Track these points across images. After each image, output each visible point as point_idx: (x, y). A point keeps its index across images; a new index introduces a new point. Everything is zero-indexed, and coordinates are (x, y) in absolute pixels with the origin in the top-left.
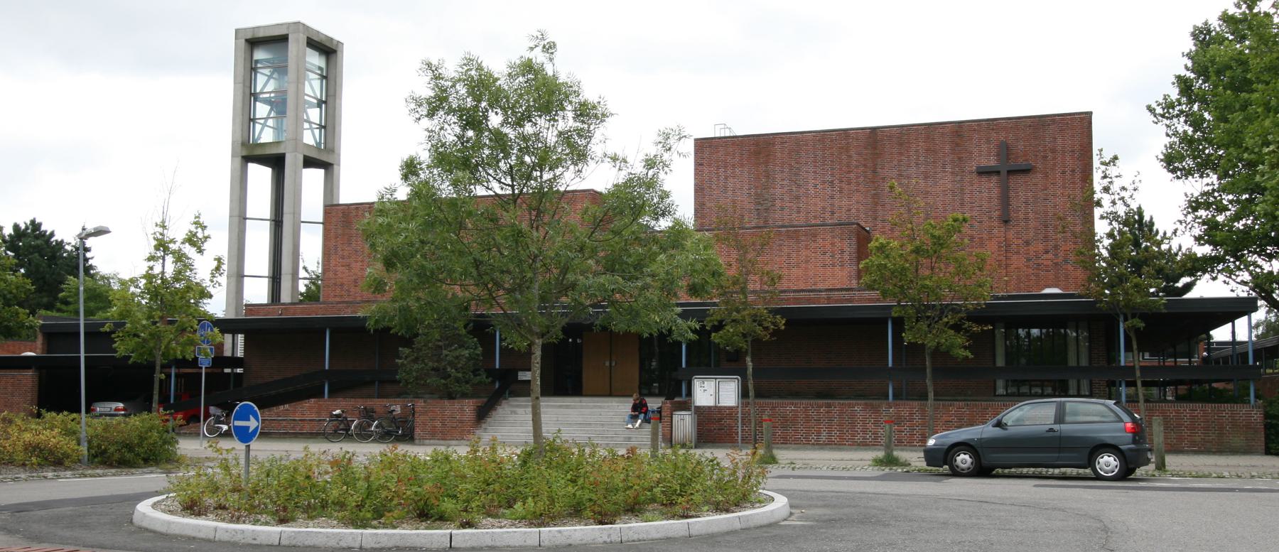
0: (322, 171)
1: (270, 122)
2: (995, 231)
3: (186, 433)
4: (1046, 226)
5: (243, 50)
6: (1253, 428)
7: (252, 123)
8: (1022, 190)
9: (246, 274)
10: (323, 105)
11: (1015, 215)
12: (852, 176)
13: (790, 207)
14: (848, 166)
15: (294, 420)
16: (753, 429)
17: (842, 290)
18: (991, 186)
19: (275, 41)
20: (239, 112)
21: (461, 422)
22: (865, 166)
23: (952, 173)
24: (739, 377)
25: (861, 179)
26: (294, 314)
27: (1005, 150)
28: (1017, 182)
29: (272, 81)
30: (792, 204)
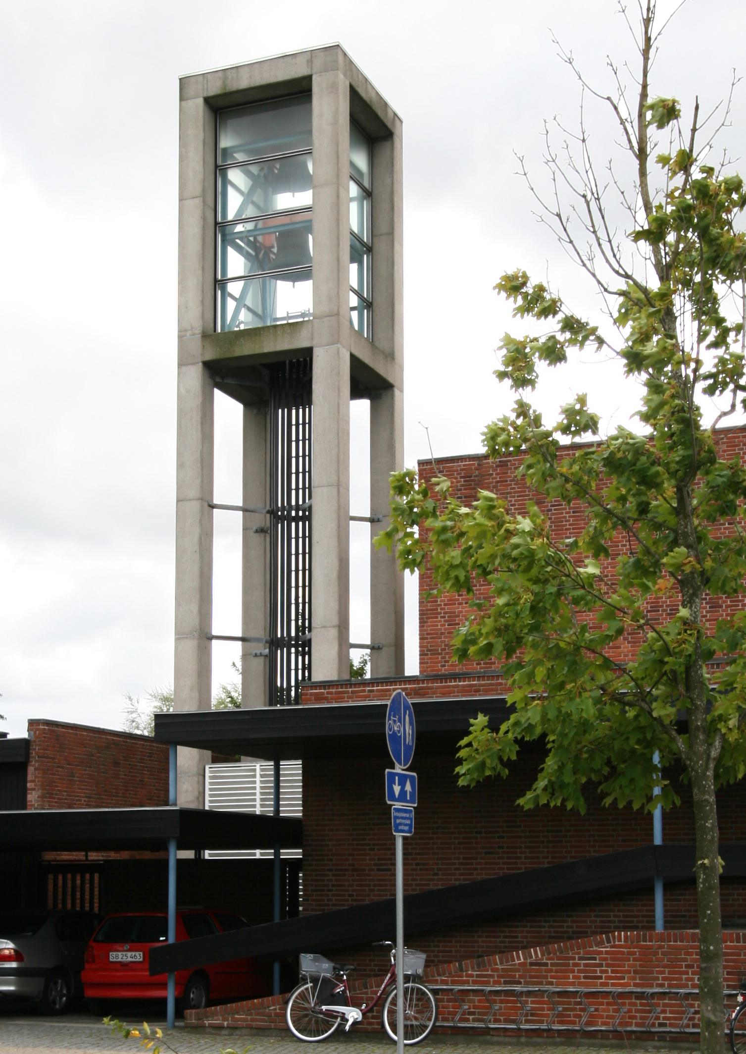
3: (220, 1028)
5: (200, 123)
9: (240, 643)
20: (194, 262)
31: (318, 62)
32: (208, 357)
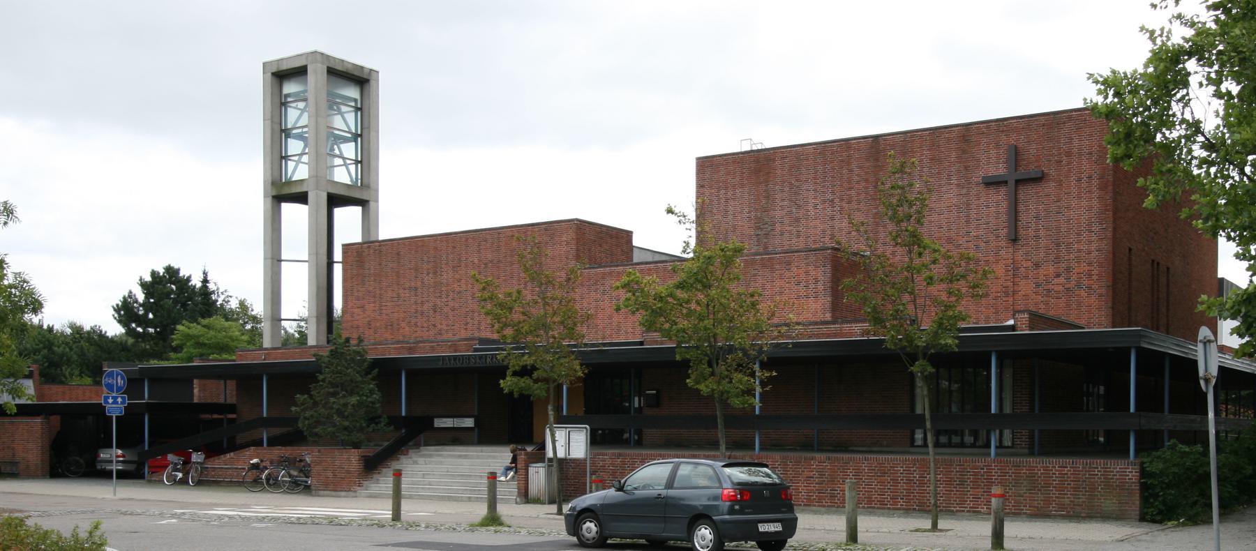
0: (359, 209)
1: (305, 158)
2: (1003, 252)
3: (155, 481)
4: (1058, 245)
6: (1128, 489)
7: (284, 161)
8: (1032, 201)
9: (282, 318)
10: (359, 139)
11: (1024, 232)
12: (853, 193)
13: (790, 232)
14: (849, 182)
15: (237, 468)
16: (932, 479)
17: (816, 323)
18: (998, 201)
19: (299, 72)
21: (348, 472)
22: (867, 181)
23: (958, 185)
24: (587, 426)
25: (863, 196)
26: (276, 359)
27: (1016, 155)
28: (1027, 193)
29: (306, 114)
30: (791, 228)
31: (310, 58)
32: (274, 194)
